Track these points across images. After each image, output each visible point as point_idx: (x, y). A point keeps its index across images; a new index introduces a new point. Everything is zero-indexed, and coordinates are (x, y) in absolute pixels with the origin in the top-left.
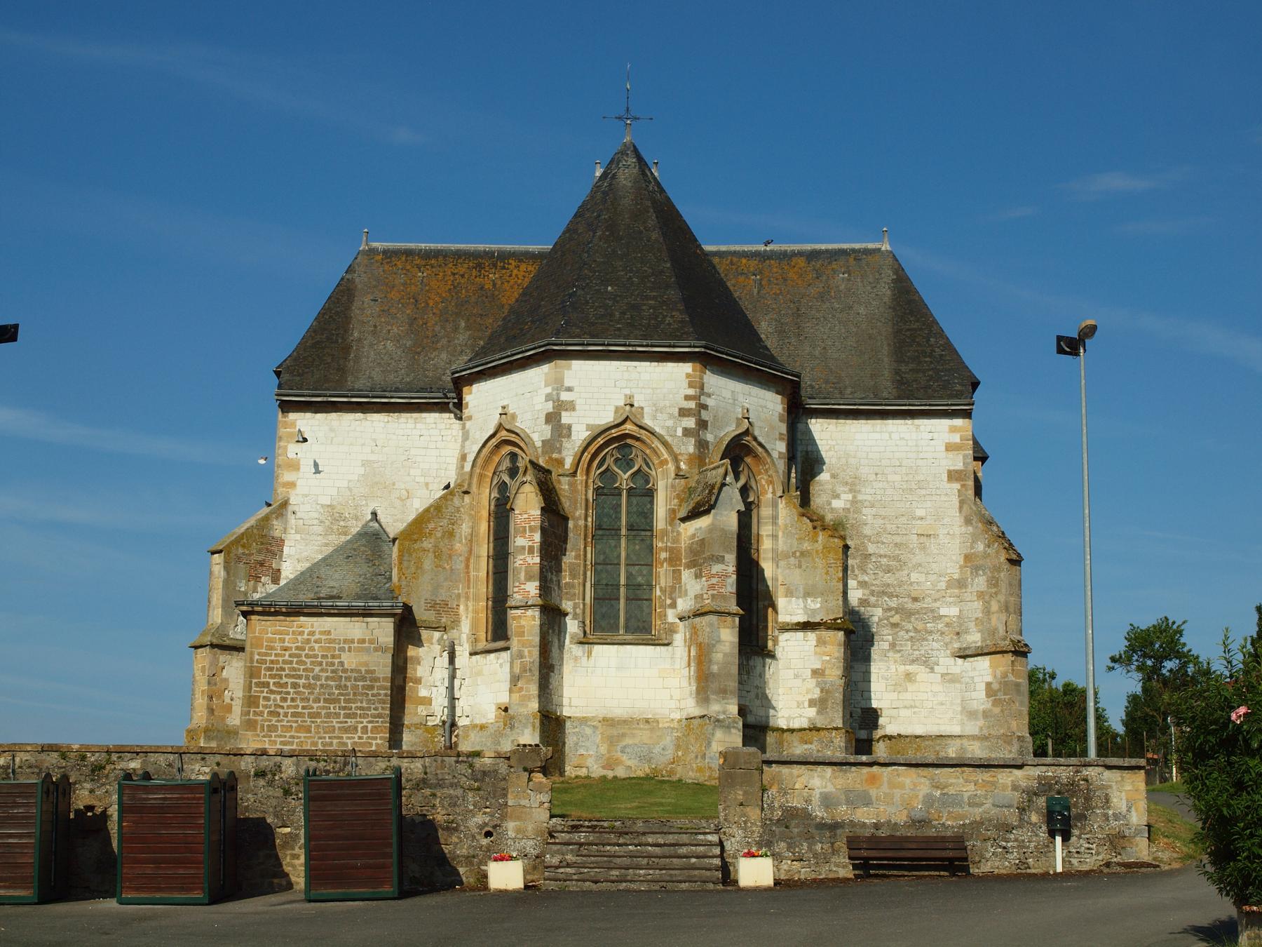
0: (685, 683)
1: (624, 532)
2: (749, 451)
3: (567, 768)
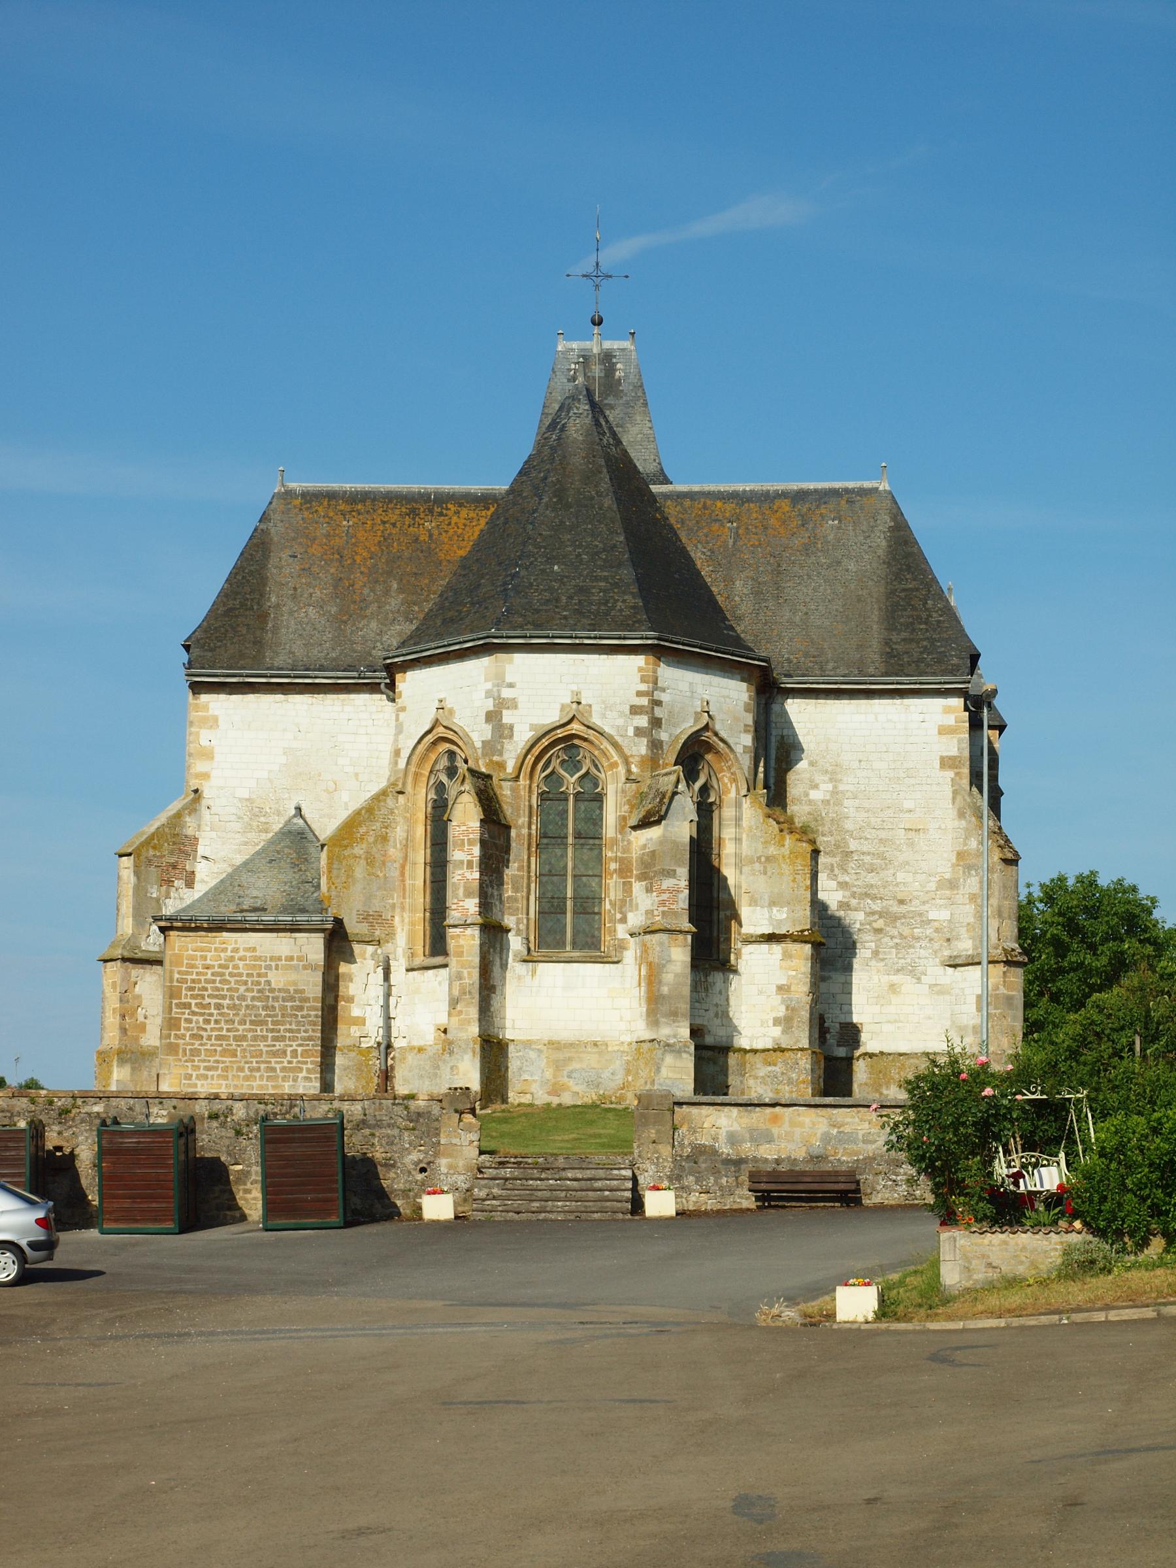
0: (635, 1003)
1: (570, 840)
2: (709, 747)
3: (511, 1094)
